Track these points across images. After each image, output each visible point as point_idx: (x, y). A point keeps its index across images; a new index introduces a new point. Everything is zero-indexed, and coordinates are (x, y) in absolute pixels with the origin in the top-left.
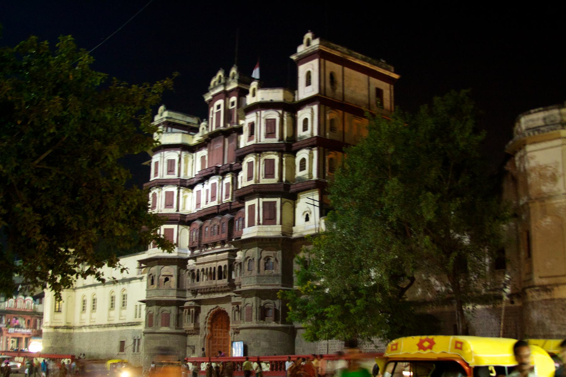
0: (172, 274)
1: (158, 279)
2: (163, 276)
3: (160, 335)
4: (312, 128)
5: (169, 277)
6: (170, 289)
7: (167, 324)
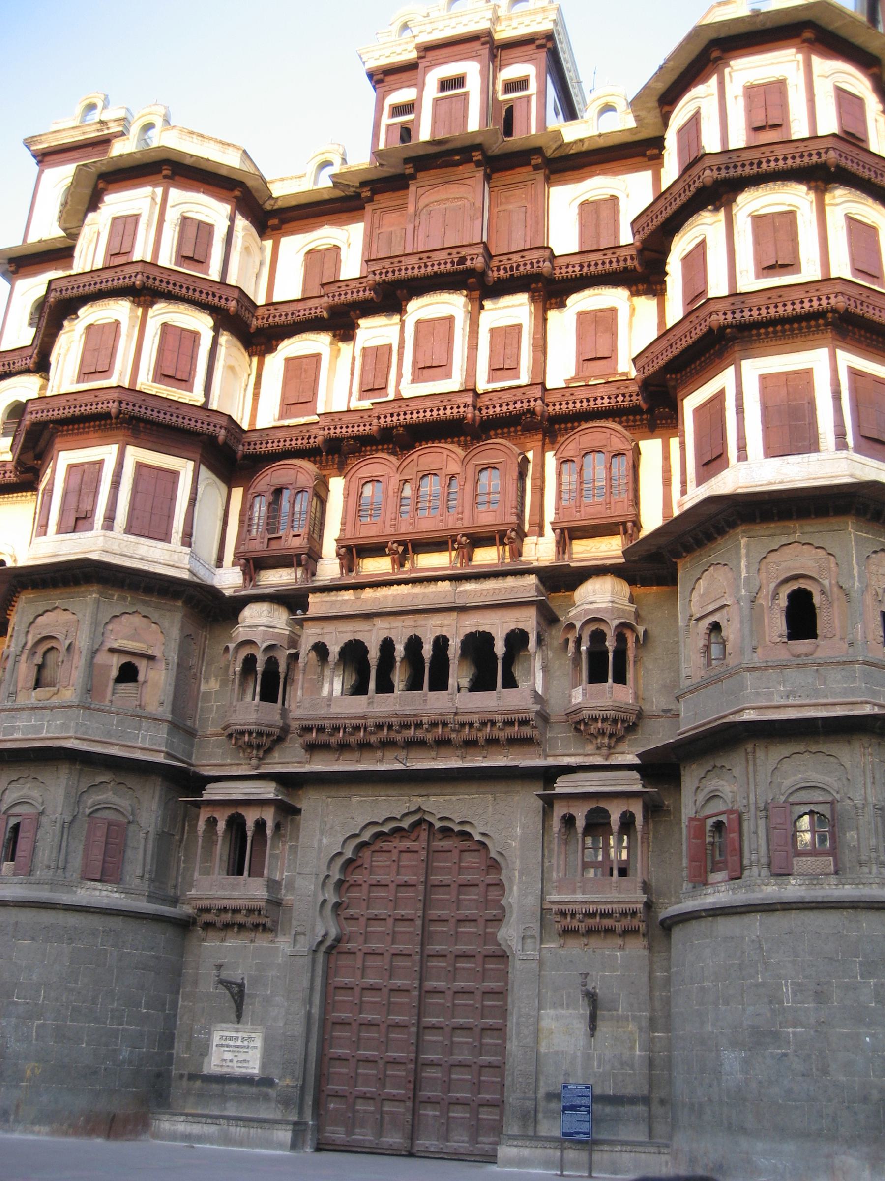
0: (156, 652)
1: (91, 664)
2: (112, 650)
3: (73, 920)
4: (473, 347)
5: (142, 665)
6: (141, 716)
7: (108, 873)
